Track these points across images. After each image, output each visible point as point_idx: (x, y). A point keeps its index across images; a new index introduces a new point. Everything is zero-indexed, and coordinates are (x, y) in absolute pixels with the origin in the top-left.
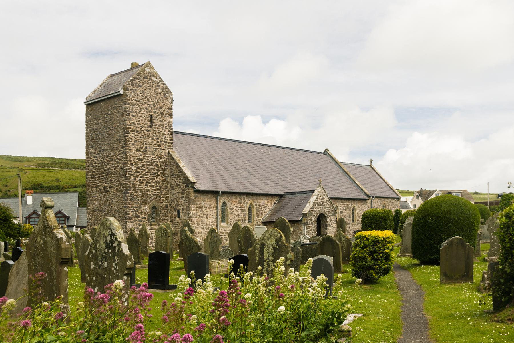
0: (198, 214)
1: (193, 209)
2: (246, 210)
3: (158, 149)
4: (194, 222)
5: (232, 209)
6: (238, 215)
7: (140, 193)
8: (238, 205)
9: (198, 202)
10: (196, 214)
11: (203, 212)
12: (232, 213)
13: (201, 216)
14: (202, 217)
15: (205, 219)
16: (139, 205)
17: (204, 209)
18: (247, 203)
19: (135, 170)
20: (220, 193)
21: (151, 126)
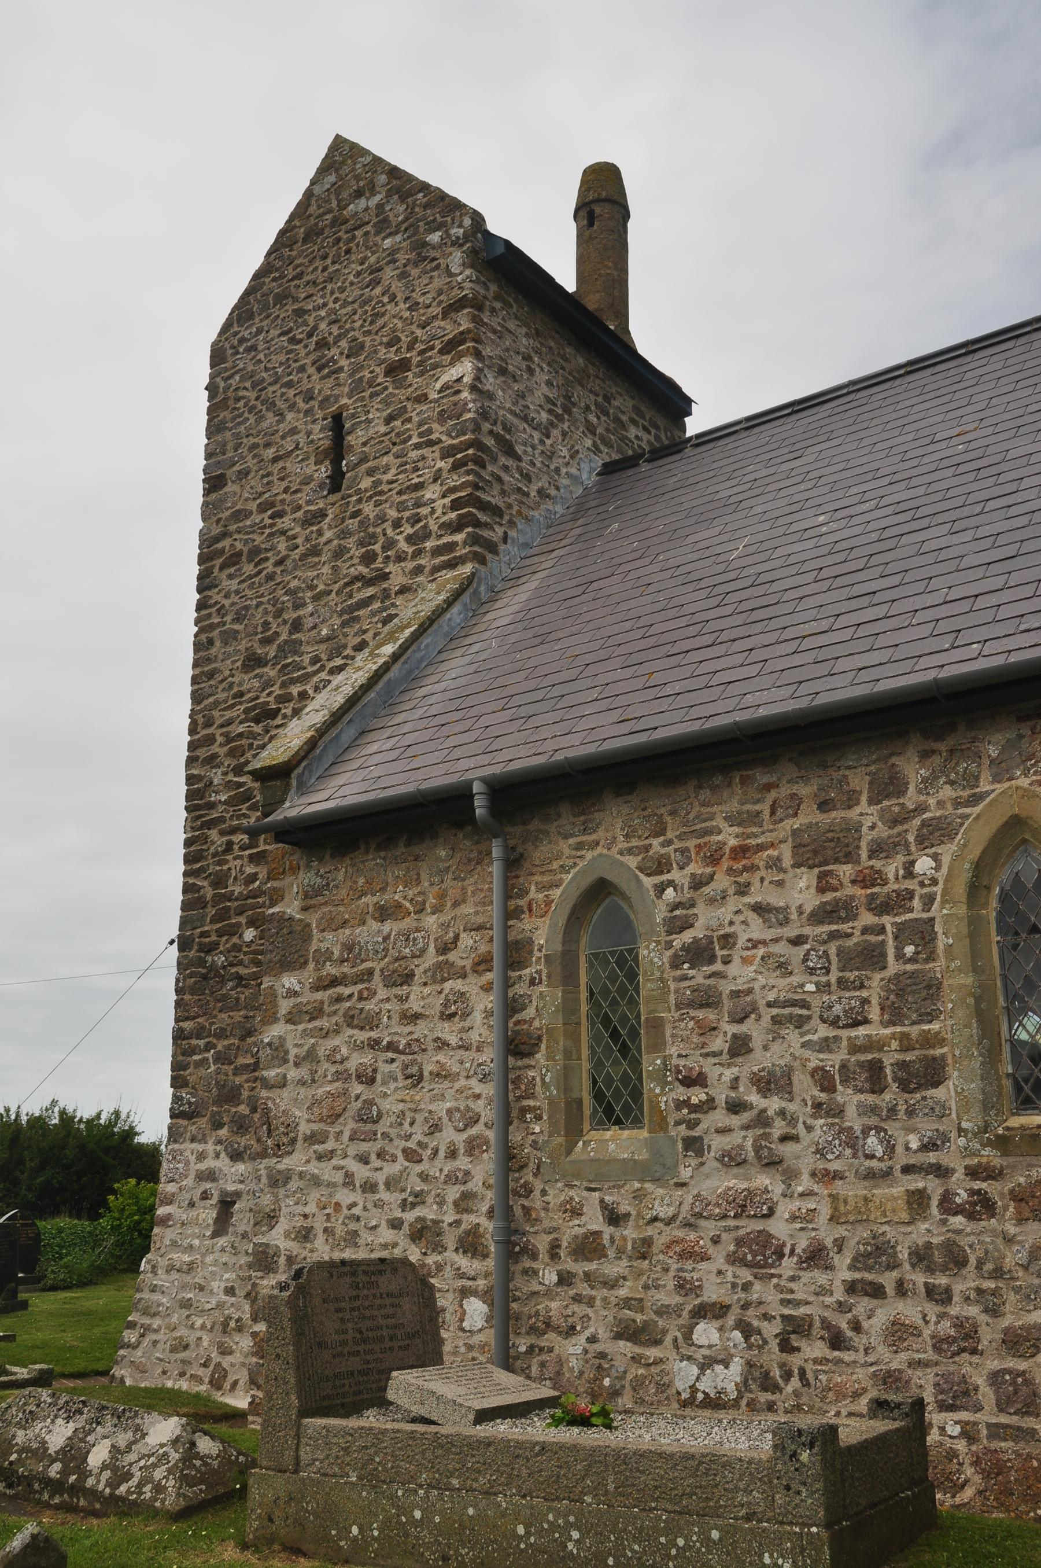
0: (325, 1047)
1: (285, 1006)
2: (923, 934)
3: (365, 603)
4: (291, 1127)
5: (699, 954)
6: (792, 1014)
7: (249, 934)
8: (801, 891)
9: (330, 941)
10: (311, 1056)
11: (371, 1022)
12: (707, 1000)
13: (357, 1061)
14: (368, 1079)
15: (390, 1099)
16: (238, 1016)
17: (382, 999)
18: (934, 834)
19: (228, 785)
20: (480, 807)
21: (336, 482)
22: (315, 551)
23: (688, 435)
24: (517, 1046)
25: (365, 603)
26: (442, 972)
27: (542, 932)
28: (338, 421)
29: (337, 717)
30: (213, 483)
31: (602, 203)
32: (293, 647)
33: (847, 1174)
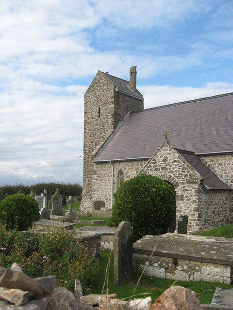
10: (97, 183)
13: (101, 184)
21: (99, 116)
22: (97, 124)
23: (144, 109)
24: (114, 183)
25: (102, 131)
26: (108, 176)
27: (116, 174)
28: (99, 108)
29: (132, 97)
30: (85, 113)
31: (133, 72)
32: (95, 135)
33: (203, 219)
